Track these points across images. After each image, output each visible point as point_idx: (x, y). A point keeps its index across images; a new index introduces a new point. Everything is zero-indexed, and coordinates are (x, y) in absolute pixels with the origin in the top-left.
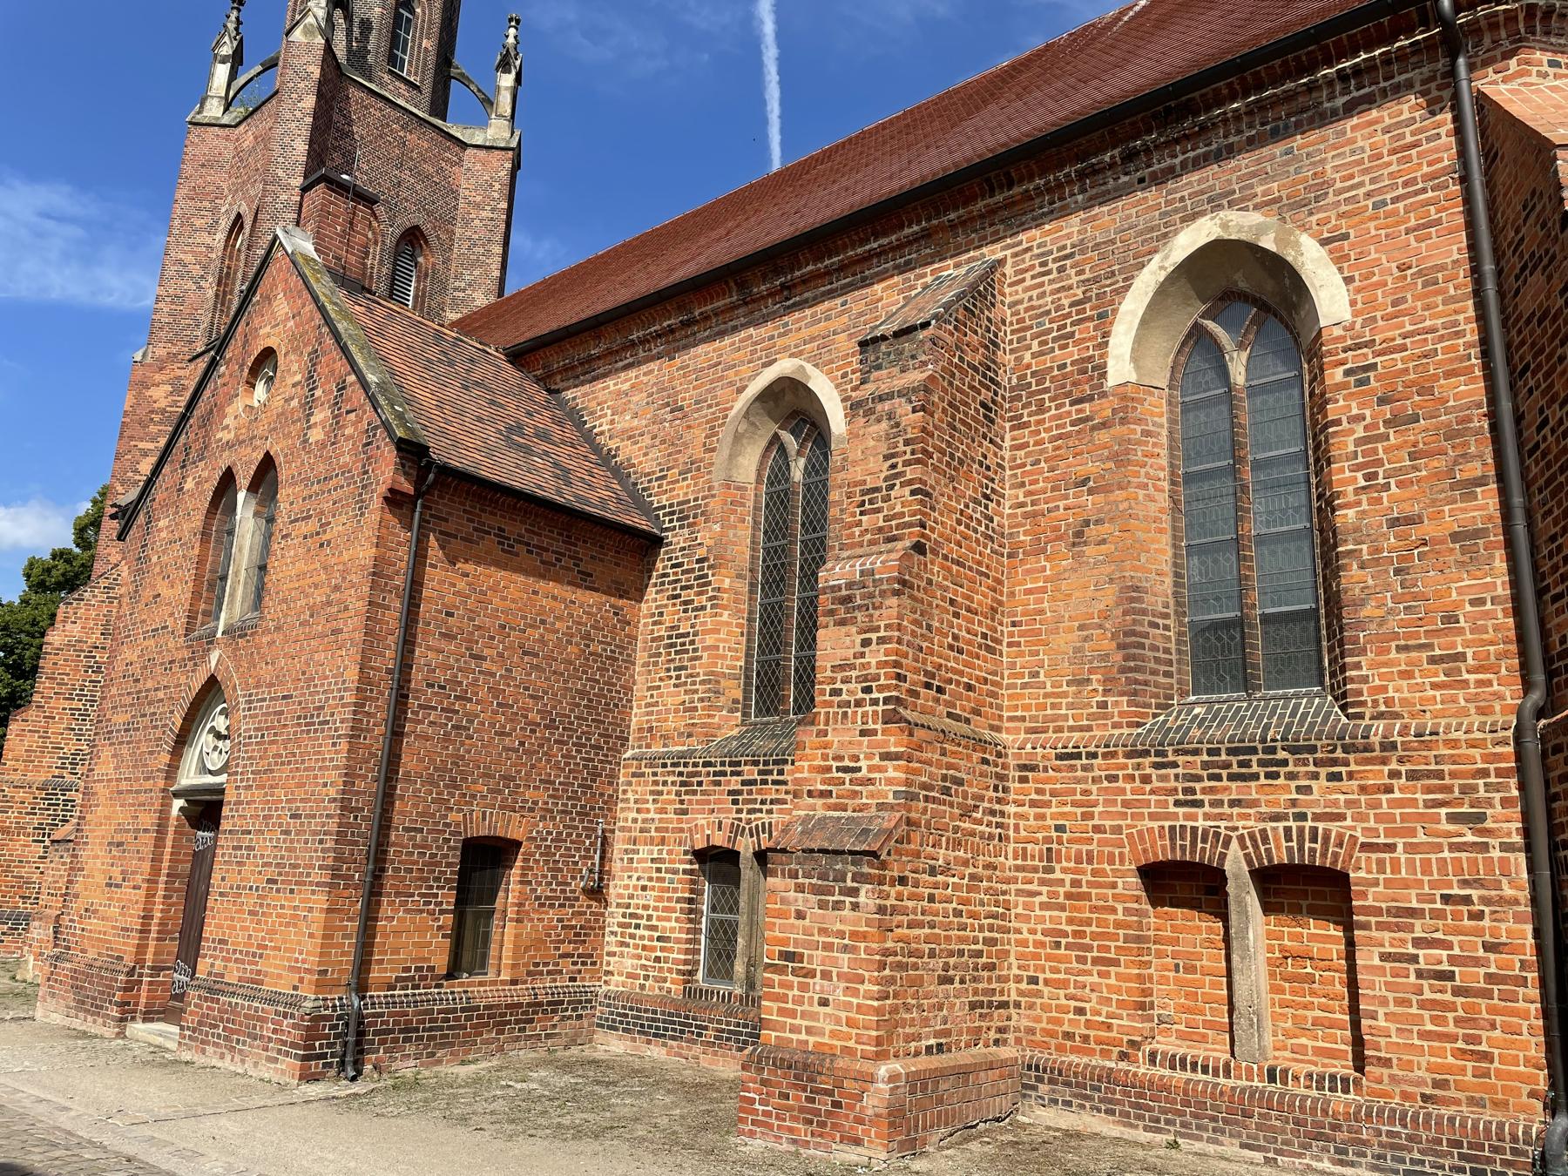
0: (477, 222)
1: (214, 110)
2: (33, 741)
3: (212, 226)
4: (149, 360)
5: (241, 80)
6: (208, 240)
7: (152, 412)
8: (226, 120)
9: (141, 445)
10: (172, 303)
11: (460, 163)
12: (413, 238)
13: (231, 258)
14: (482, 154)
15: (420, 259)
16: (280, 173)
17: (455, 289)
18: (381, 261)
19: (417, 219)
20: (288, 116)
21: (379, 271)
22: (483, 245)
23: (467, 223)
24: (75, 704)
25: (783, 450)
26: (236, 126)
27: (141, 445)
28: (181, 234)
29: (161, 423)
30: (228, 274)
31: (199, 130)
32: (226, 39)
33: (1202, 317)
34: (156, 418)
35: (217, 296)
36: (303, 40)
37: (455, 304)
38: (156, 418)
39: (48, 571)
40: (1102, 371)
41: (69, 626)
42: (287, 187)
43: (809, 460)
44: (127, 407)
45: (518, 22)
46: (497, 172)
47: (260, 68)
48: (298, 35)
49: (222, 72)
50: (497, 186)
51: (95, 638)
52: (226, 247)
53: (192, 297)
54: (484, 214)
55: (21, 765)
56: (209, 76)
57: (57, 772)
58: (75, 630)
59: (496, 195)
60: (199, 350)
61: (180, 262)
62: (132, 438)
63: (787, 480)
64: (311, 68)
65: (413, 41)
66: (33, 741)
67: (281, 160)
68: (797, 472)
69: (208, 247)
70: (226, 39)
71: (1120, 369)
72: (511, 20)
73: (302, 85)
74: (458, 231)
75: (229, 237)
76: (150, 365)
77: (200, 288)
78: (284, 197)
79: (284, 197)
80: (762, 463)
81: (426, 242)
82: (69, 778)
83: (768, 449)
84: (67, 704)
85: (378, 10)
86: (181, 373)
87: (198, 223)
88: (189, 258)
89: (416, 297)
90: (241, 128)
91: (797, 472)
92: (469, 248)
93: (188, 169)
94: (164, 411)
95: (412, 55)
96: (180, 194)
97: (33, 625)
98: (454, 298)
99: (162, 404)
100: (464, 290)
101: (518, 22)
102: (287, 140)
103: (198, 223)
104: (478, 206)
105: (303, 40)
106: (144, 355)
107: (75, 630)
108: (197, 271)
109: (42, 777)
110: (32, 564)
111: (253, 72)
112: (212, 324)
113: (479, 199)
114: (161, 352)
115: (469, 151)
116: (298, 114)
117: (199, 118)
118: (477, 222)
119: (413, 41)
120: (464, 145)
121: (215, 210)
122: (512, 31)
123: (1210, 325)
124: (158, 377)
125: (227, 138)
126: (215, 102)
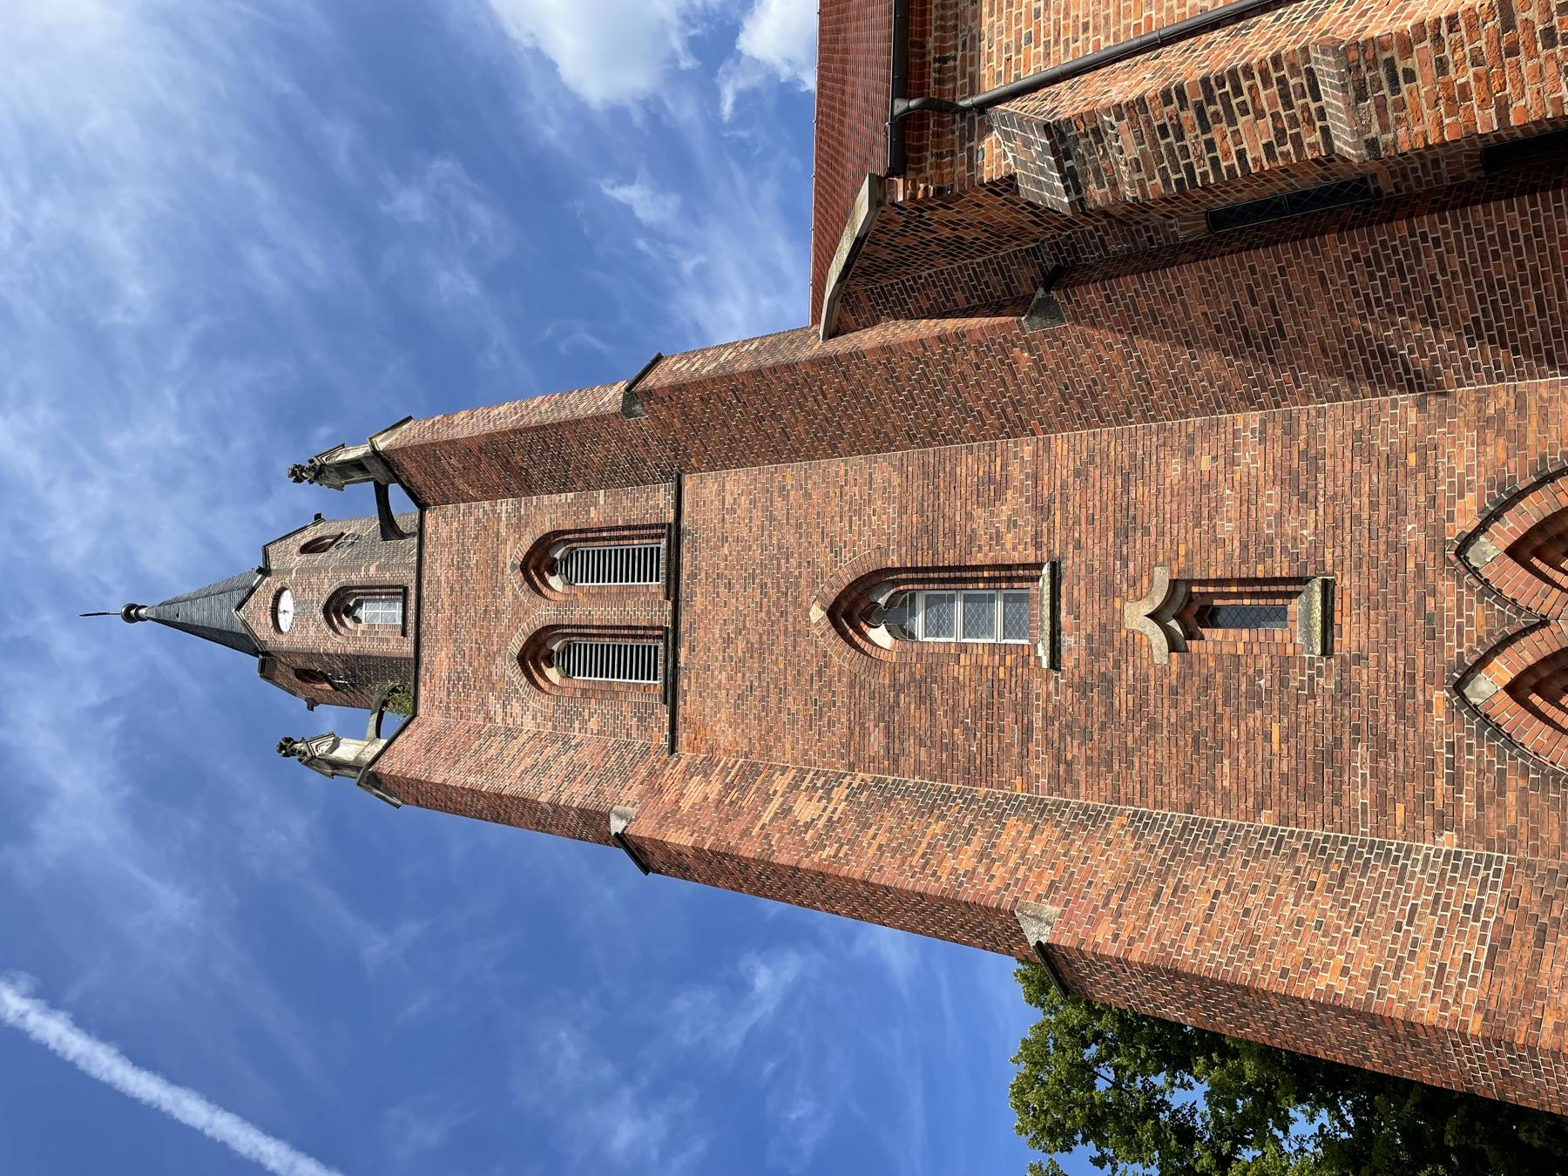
26: (415, 715)
86: (683, 763)
94: (728, 787)
125: (419, 725)
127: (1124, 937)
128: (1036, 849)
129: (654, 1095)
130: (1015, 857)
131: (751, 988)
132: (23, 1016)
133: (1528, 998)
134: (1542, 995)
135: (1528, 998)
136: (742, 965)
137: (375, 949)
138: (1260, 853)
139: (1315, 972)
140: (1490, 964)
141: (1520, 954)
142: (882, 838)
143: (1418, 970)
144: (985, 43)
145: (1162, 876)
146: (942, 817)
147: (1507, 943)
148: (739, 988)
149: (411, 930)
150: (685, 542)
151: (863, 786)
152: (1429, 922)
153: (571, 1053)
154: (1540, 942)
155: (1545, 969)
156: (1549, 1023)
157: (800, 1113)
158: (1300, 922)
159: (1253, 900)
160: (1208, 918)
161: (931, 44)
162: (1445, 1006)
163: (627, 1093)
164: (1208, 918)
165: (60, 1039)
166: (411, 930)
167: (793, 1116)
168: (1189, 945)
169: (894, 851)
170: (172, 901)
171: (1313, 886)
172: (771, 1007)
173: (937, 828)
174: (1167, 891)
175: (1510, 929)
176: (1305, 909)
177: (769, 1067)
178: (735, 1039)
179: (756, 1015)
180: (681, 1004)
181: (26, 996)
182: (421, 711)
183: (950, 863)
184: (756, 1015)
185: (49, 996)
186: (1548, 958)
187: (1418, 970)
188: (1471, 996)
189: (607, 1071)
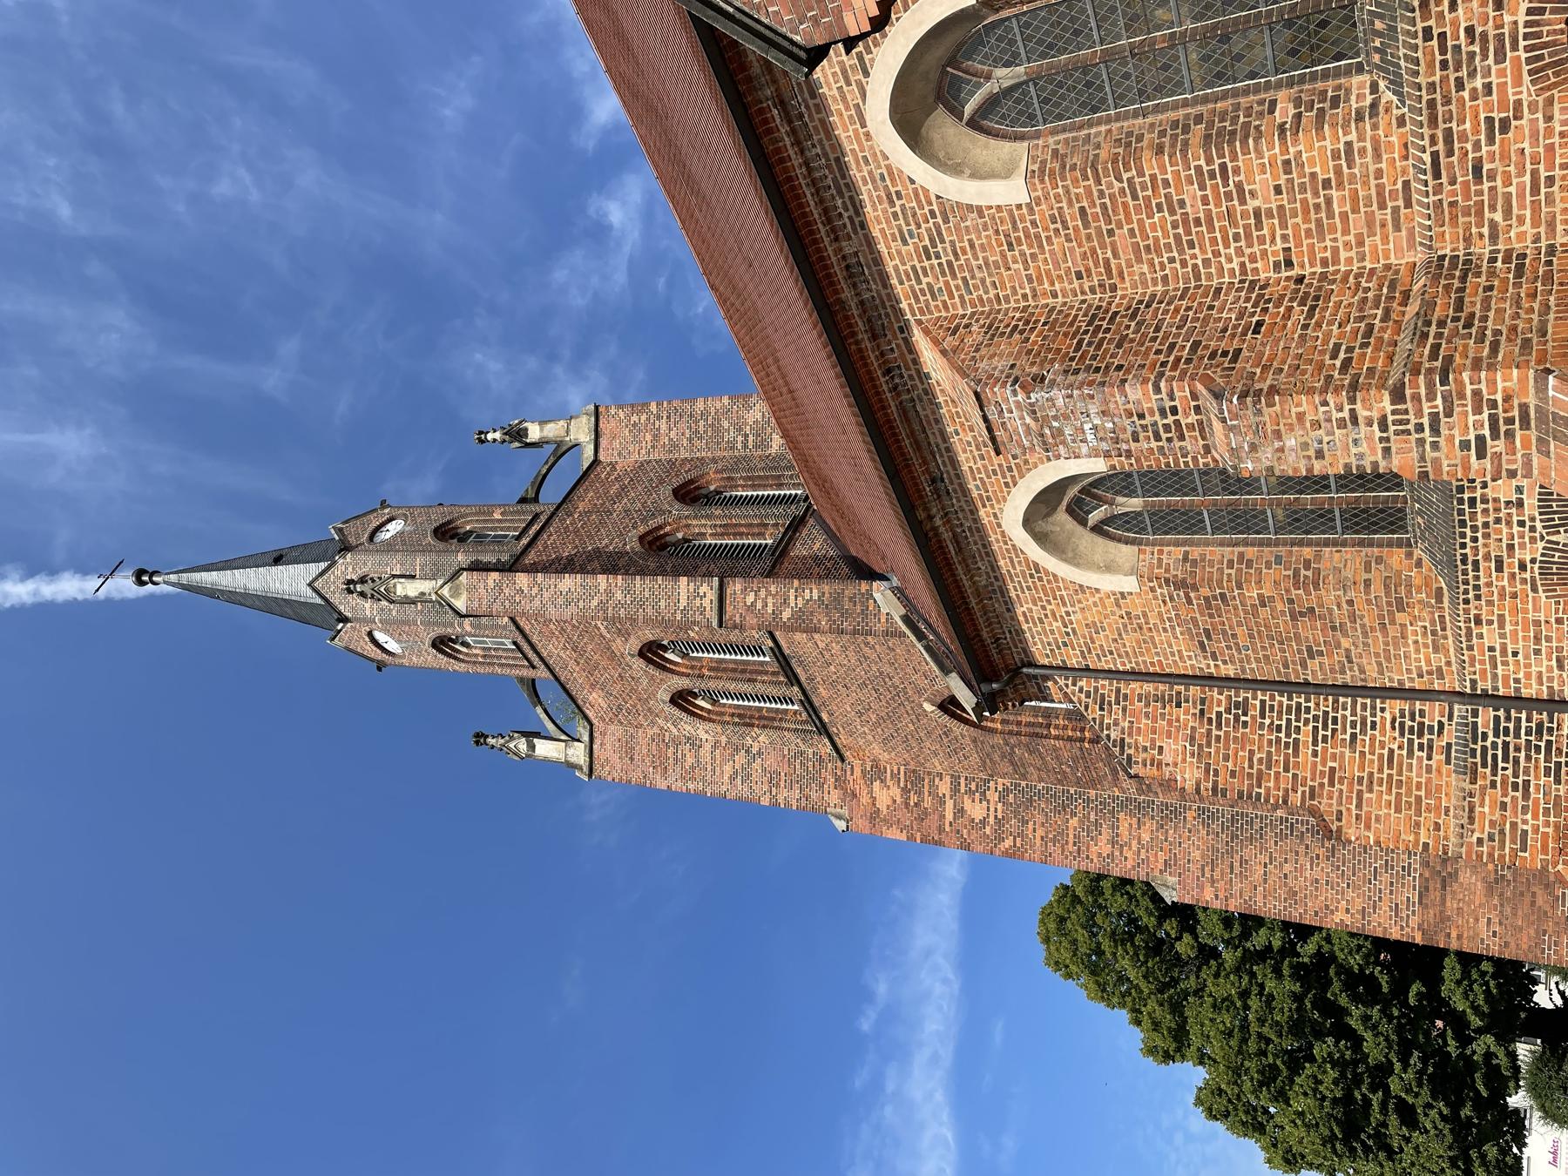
0: (672, 434)
1: (578, 753)
2: (1379, 802)
3: (692, 745)
4: (845, 812)
5: (550, 726)
6: (708, 747)
7: (907, 805)
8: (586, 738)
9: (949, 816)
10: (778, 786)
11: (613, 465)
12: (689, 494)
13: (722, 714)
14: (603, 442)
15: (712, 488)
16: (595, 603)
17: (745, 446)
18: (708, 517)
19: (666, 491)
20: (537, 602)
21: (719, 517)
22: (696, 422)
23: (675, 446)
24: (1306, 735)
25: (992, 103)
26: (591, 725)
27: (949, 816)
28: (704, 780)
29: (919, 793)
30: (739, 716)
31: (596, 766)
32: (512, 745)
33: (960, 117)
34: (914, 799)
35: (764, 727)
36: (464, 597)
37: (763, 443)
38: (914, 799)
39: (1156, 1026)
40: (1012, 213)
41: (1167, 757)
42: (609, 592)
43: (1117, 493)
44: (903, 837)
45: (481, 433)
46: (621, 421)
47: (539, 710)
48: (460, 604)
49: (544, 749)
50: (635, 418)
51: (1185, 716)
52: (711, 720)
53: (771, 761)
54: (664, 427)
55: (1427, 819)
56: (546, 762)
57: (1438, 757)
58: (1172, 748)
59: (644, 417)
60: (829, 749)
61: (732, 778)
62: (941, 830)
63: (1140, 514)
64: (491, 583)
65: (495, 529)
66: (1379, 802)
67: (581, 604)
68: (1134, 504)
69: (715, 747)
70: (512, 745)
71: (1010, 192)
72: (481, 441)
73: (507, 591)
74: (684, 454)
75: (700, 717)
76: (851, 810)
77: (759, 753)
78: (619, 595)
79: (619, 595)
80: (1119, 540)
81: (691, 481)
82: (1450, 735)
83: (988, 132)
84: (1306, 752)
85: (460, 557)
86: (857, 771)
87: (690, 760)
88: (728, 769)
89: (754, 487)
90: (590, 714)
91: (1134, 504)
92: (700, 438)
93: (636, 776)
94: (905, 790)
95: (508, 529)
96: (662, 785)
97: (1230, 1034)
98: (756, 446)
99: (896, 792)
100: (746, 436)
101: (481, 433)
102: (560, 601)
103: (690, 760)
104: (656, 437)
105: (464, 597)
106: (839, 817)
107: (1172, 748)
108: (741, 758)
109: (1452, 782)
110: (1151, 1051)
111: (543, 716)
112: (796, 730)
113: (649, 437)
114: (834, 797)
115: (602, 458)
116: (535, 590)
117: (586, 769)
118: (672, 434)
119: (495, 529)
120: (596, 462)
121: (676, 743)
122: (490, 436)
123: (969, 109)
124: (865, 799)
125: (603, 734)
126: (570, 752)
127: (1221, 896)
128: (1146, 837)
129: (582, 355)
130: (1134, 843)
131: (610, 227)
132: (36, 593)
133: (1442, 921)
134: (1449, 919)
135: (1442, 921)
136: (591, 211)
137: (273, 380)
138: (1282, 836)
139: (1332, 912)
140: (1420, 902)
141: (1435, 895)
142: (1040, 832)
143: (1384, 907)
144: (1028, 635)
145: (1230, 852)
146: (1073, 814)
147: (1427, 889)
148: (600, 232)
149: (289, 348)
150: (793, 662)
151: (1006, 790)
152: (1385, 878)
153: (495, 366)
154: (1444, 888)
155: (1448, 904)
156: (1454, 934)
157: (705, 303)
158: (1317, 881)
159: (1287, 868)
160: (1265, 881)
161: (985, 635)
162: (1402, 928)
163: (558, 370)
164: (1265, 881)
165: (82, 591)
166: (289, 348)
167: (700, 310)
168: (1259, 898)
169: (1054, 841)
170: (71, 442)
171: (1318, 857)
172: (636, 234)
173: (1074, 822)
174: (1236, 865)
175: (1427, 880)
176: (1316, 873)
177: (661, 283)
178: (620, 278)
179: (627, 249)
180: (560, 275)
181: (23, 580)
182: (595, 722)
183: (1094, 849)
184: (627, 249)
185: (38, 565)
186: (1449, 898)
187: (1384, 907)
188: (1414, 921)
189: (532, 363)
